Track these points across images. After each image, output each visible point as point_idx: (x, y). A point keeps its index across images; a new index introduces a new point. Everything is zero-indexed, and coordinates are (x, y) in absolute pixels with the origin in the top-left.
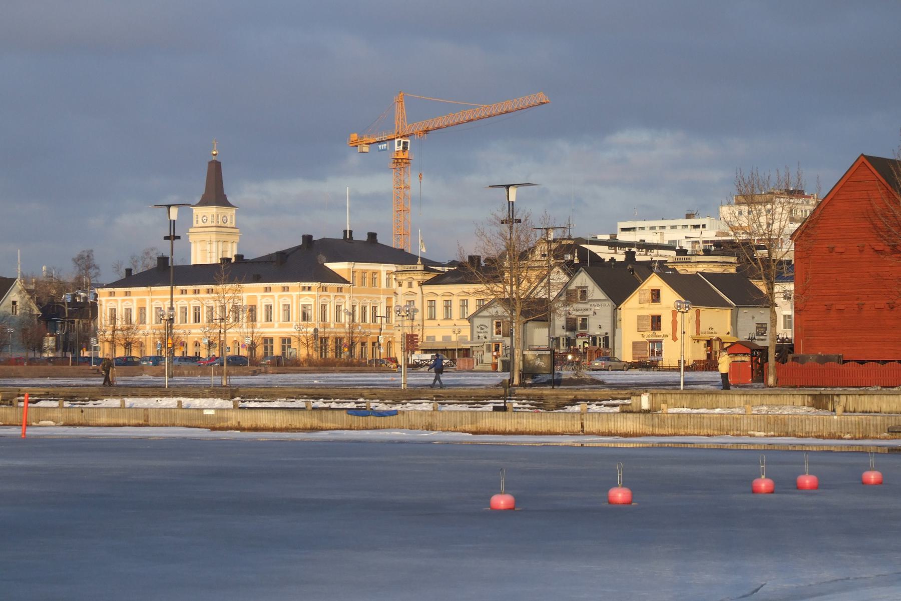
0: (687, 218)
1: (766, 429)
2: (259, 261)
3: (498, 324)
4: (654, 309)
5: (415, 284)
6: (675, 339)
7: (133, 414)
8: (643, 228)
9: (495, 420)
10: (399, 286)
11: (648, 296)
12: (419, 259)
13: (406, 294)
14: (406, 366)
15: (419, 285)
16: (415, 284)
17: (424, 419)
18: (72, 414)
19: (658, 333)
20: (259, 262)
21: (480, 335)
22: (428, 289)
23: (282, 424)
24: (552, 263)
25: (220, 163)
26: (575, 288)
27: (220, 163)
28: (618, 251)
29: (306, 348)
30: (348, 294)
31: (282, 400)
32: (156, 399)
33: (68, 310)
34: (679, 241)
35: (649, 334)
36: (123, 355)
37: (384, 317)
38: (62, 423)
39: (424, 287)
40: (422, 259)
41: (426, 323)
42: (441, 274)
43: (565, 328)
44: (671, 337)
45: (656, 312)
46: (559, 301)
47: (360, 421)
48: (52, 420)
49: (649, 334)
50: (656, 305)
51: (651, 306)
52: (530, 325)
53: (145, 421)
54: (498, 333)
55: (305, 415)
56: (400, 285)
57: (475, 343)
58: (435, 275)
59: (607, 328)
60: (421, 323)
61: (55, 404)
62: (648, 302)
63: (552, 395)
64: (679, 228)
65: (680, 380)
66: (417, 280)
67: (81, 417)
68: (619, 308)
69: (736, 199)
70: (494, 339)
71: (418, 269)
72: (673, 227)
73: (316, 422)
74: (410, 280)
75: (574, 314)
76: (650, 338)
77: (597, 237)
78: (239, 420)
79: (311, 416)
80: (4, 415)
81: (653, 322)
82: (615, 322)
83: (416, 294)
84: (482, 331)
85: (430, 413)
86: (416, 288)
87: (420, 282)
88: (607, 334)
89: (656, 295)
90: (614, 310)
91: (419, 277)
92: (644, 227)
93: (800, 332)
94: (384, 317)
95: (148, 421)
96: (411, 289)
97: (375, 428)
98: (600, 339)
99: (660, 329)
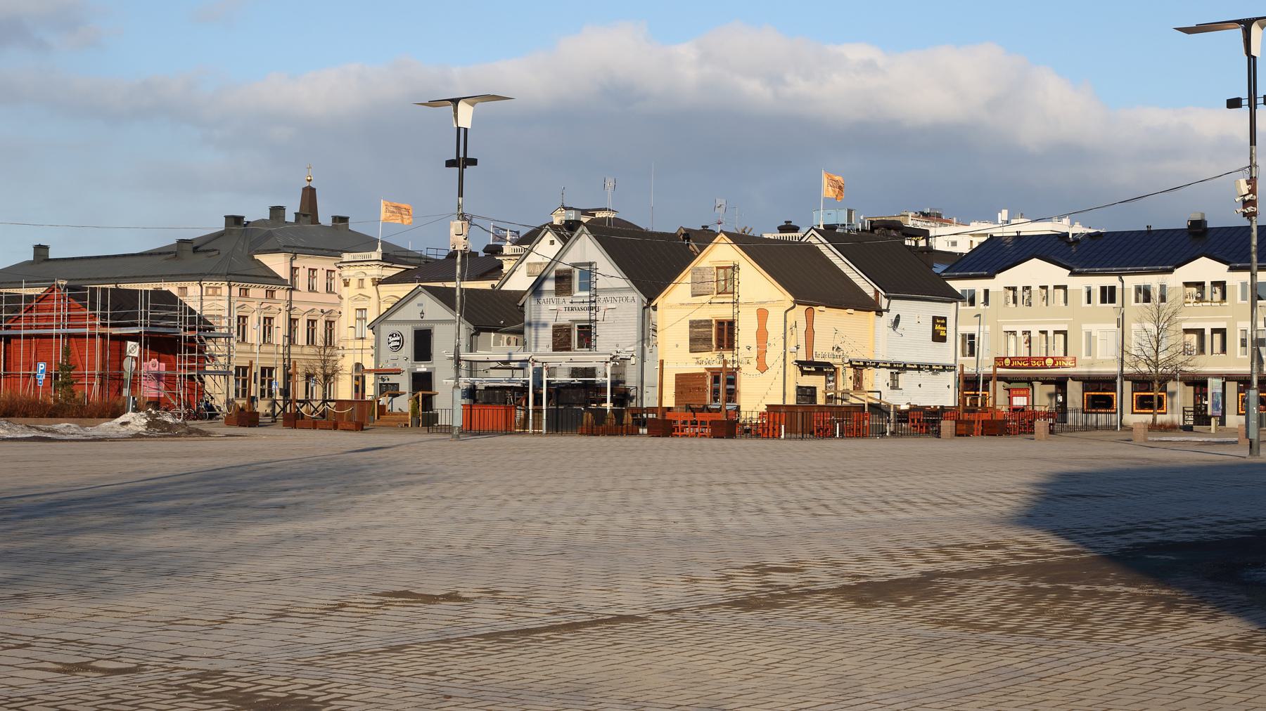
2: (161, 251)
5: (368, 283)
6: (762, 368)
12: (380, 244)
14: (1117, 401)
15: (373, 285)
18: (816, 410)
20: (160, 254)
25: (315, 189)
27: (315, 189)
33: (547, 381)
39: (381, 287)
40: (385, 244)
42: (413, 267)
44: (754, 363)
49: (711, 359)
56: (346, 284)
58: (403, 270)
68: (653, 304)
71: (372, 259)
74: (362, 276)
82: (647, 332)
83: (370, 298)
86: (369, 289)
87: (375, 279)
90: (644, 308)
91: (376, 271)
96: (362, 291)
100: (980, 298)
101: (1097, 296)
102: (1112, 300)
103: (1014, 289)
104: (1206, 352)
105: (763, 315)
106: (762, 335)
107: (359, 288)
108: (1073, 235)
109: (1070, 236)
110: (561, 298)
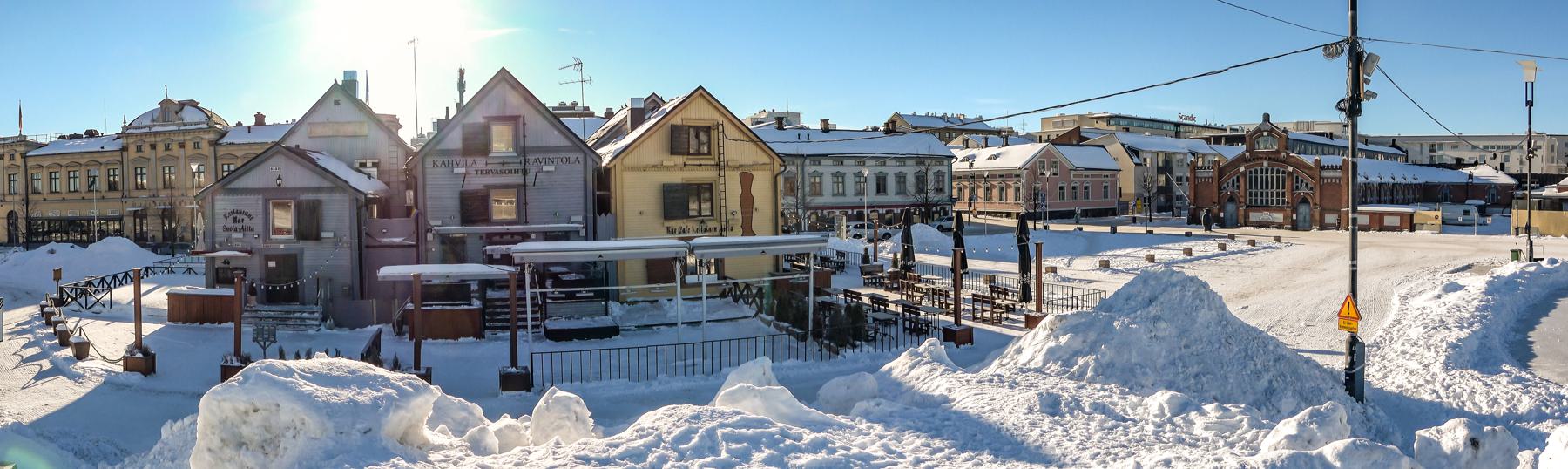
26: (482, 121)
29: (132, 218)
36: (134, 324)
37: (1352, 107)
46: (449, 165)
61: (1072, 228)
65: (624, 237)
84: (239, 226)
93: (386, 240)
94: (1352, 107)
105: (746, 179)
106: (747, 200)
110: (470, 160)
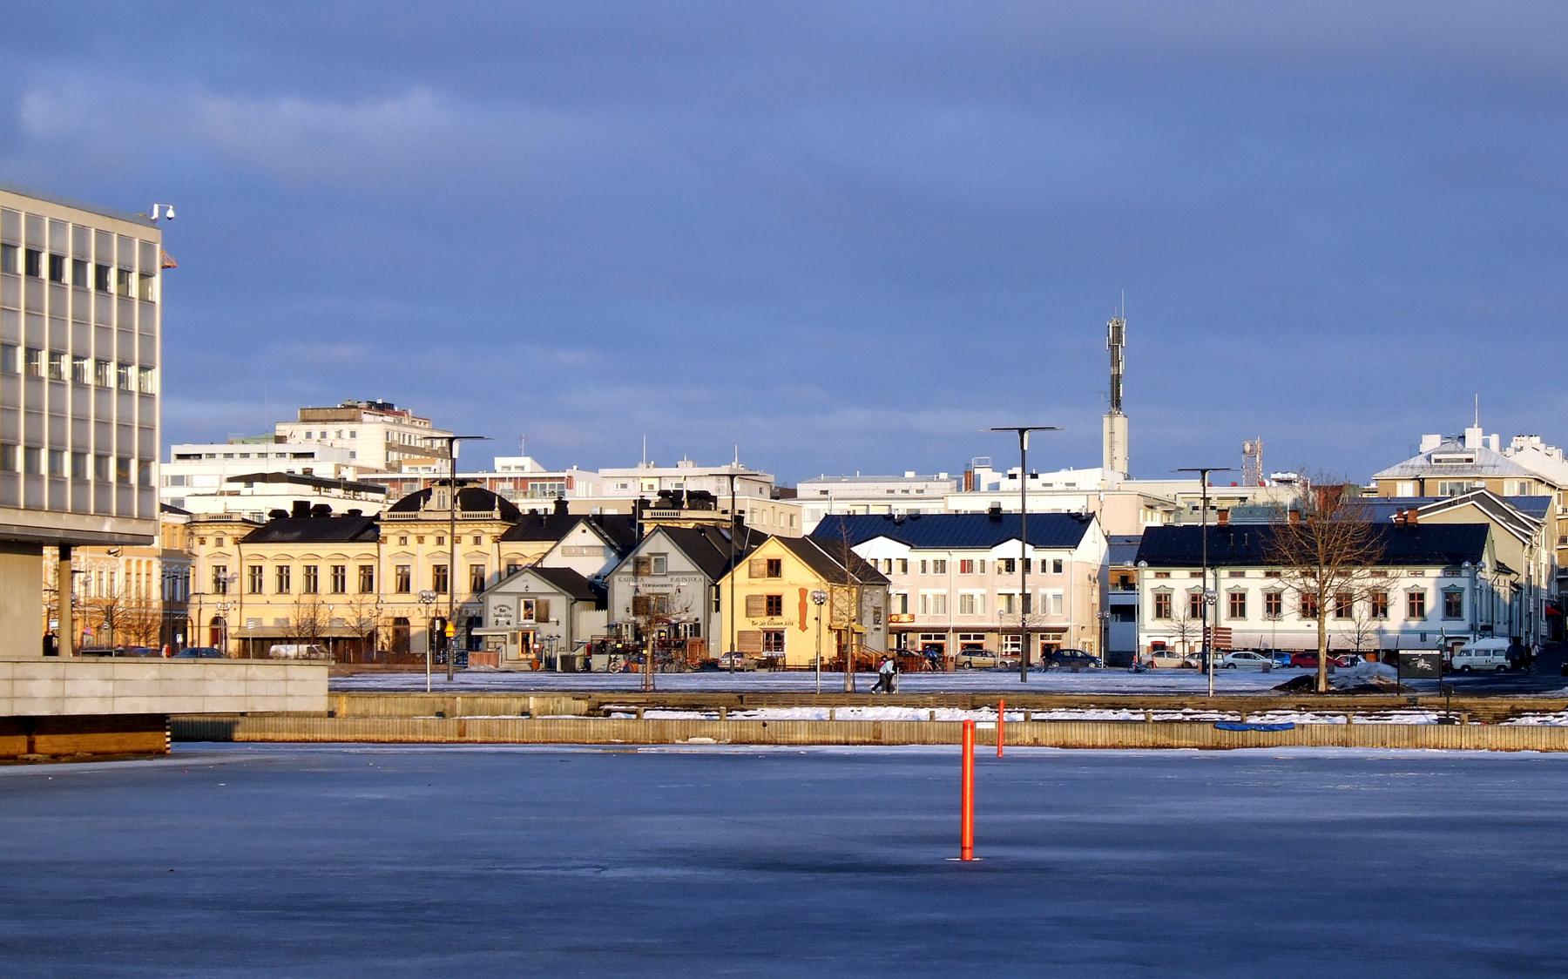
0: (276, 442)
1: (437, 732)
3: (528, 605)
4: (771, 587)
5: (228, 541)
6: (803, 627)
7: (855, 730)
8: (212, 456)
9: (1069, 730)
10: (420, 542)
11: (764, 567)
13: (213, 556)
15: (494, 542)
16: (228, 541)
17: (1335, 734)
19: (777, 619)
21: (500, 619)
22: (250, 549)
23: (1108, 740)
24: (458, 515)
28: (323, 494)
30: (84, 554)
31: (1060, 710)
32: (852, 708)
34: (167, 485)
35: (765, 622)
38: (729, 740)
39: (244, 547)
41: (246, 599)
43: (631, 611)
45: (774, 591)
47: (1237, 736)
48: (711, 737)
49: (765, 622)
50: (773, 581)
51: (767, 583)
52: (578, 605)
53: (874, 738)
54: (529, 616)
55: (1146, 729)
56: (202, 542)
57: (492, 631)
59: (698, 612)
60: (238, 599)
62: (762, 576)
63: (1477, 704)
64: (237, 456)
66: (232, 535)
67: (762, 733)
69: (303, 414)
70: (523, 626)
72: (245, 455)
73: (1162, 739)
75: (644, 591)
76: (765, 627)
77: (410, 468)
78: (1035, 736)
79: (1155, 731)
80: (623, 731)
81: (770, 604)
84: (503, 614)
85: (1344, 727)
88: (697, 619)
89: (774, 568)
92: (214, 454)
95: (880, 738)
96: (220, 549)
97: (1259, 746)
98: (686, 627)
99: (779, 614)
100: (977, 566)
101: (930, 567)
102: (943, 571)
103: (890, 560)
104: (46, 657)
107: (218, 546)
108: (898, 515)
109: (896, 517)
